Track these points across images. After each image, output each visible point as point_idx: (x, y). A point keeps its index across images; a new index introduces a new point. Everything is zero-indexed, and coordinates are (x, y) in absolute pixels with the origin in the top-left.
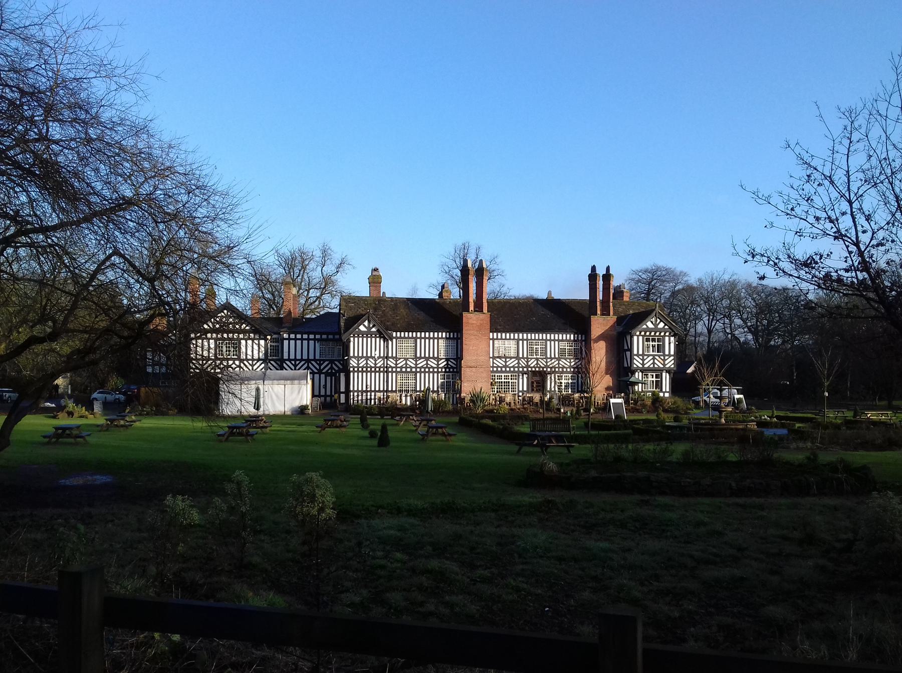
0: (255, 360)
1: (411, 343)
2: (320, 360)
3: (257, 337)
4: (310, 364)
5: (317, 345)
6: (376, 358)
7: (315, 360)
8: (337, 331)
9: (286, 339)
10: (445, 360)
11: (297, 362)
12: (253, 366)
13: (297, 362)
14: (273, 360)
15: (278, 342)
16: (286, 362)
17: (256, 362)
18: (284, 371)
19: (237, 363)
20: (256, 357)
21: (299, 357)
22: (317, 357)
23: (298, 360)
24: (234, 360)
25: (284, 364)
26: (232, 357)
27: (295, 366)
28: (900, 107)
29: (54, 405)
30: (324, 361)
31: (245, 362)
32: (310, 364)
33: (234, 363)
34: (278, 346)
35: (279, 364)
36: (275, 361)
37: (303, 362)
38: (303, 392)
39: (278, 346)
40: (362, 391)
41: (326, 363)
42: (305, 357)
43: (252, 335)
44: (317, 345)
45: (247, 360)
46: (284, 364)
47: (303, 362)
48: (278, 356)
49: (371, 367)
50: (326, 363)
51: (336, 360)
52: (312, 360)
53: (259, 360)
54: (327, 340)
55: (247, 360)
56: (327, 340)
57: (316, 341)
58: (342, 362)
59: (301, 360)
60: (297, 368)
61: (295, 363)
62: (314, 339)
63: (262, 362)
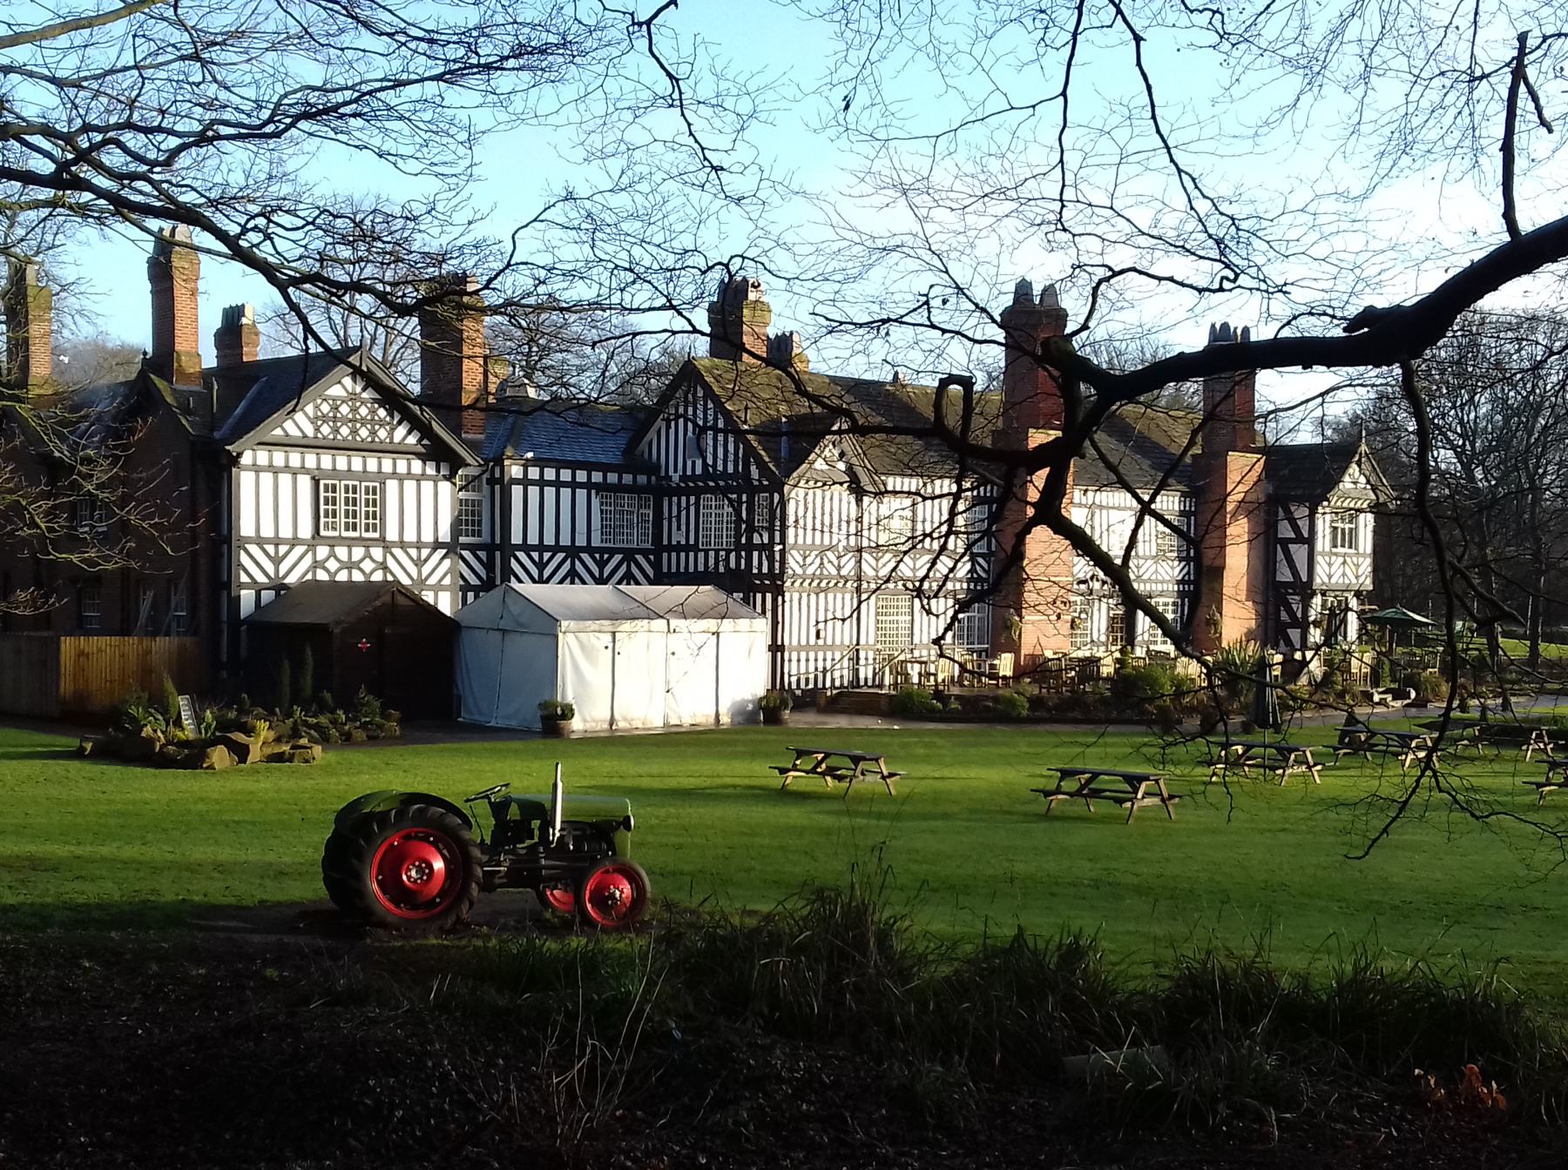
0: (426, 545)
1: (360, 459)
2: (601, 550)
3: (430, 470)
4: (577, 562)
5: (595, 502)
6: (841, 549)
7: (589, 549)
8: (1147, 517)
9: (517, 482)
10: (272, 574)
11: (547, 556)
12: (419, 563)
13: (547, 556)
14: (466, 547)
15: (480, 490)
16: (517, 553)
17: (287, 547)
18: (578, 587)
19: (377, 553)
20: (428, 537)
21: (549, 540)
22: (596, 542)
23: (548, 549)
24: (366, 543)
25: (513, 560)
26: (345, 534)
27: (541, 566)
28: (1526, 225)
29: (309, 651)
30: (612, 552)
31: (585, 556)
32: (577, 562)
33: (368, 555)
34: (480, 502)
35: (242, 573)
36: (472, 548)
37: (560, 556)
38: (563, 654)
39: (480, 502)
40: (808, 648)
41: (618, 557)
42: (565, 540)
43: (417, 466)
44: (595, 502)
45: (403, 545)
46: (513, 560)
47: (560, 556)
48: (480, 536)
49: (830, 578)
50: (618, 557)
51: (640, 551)
52: (583, 550)
53: (437, 545)
54: (619, 488)
55: (403, 545)
56: (619, 488)
57: (593, 492)
58: (652, 557)
59: (556, 549)
60: (547, 573)
61: (541, 557)
62: (589, 486)
63: (444, 551)
